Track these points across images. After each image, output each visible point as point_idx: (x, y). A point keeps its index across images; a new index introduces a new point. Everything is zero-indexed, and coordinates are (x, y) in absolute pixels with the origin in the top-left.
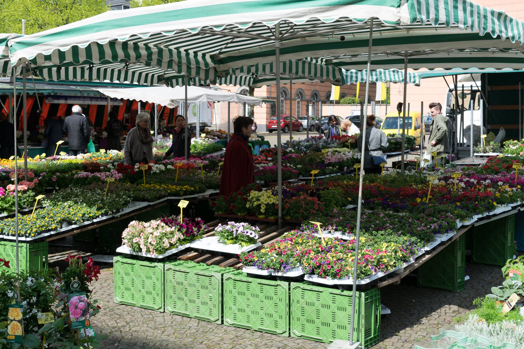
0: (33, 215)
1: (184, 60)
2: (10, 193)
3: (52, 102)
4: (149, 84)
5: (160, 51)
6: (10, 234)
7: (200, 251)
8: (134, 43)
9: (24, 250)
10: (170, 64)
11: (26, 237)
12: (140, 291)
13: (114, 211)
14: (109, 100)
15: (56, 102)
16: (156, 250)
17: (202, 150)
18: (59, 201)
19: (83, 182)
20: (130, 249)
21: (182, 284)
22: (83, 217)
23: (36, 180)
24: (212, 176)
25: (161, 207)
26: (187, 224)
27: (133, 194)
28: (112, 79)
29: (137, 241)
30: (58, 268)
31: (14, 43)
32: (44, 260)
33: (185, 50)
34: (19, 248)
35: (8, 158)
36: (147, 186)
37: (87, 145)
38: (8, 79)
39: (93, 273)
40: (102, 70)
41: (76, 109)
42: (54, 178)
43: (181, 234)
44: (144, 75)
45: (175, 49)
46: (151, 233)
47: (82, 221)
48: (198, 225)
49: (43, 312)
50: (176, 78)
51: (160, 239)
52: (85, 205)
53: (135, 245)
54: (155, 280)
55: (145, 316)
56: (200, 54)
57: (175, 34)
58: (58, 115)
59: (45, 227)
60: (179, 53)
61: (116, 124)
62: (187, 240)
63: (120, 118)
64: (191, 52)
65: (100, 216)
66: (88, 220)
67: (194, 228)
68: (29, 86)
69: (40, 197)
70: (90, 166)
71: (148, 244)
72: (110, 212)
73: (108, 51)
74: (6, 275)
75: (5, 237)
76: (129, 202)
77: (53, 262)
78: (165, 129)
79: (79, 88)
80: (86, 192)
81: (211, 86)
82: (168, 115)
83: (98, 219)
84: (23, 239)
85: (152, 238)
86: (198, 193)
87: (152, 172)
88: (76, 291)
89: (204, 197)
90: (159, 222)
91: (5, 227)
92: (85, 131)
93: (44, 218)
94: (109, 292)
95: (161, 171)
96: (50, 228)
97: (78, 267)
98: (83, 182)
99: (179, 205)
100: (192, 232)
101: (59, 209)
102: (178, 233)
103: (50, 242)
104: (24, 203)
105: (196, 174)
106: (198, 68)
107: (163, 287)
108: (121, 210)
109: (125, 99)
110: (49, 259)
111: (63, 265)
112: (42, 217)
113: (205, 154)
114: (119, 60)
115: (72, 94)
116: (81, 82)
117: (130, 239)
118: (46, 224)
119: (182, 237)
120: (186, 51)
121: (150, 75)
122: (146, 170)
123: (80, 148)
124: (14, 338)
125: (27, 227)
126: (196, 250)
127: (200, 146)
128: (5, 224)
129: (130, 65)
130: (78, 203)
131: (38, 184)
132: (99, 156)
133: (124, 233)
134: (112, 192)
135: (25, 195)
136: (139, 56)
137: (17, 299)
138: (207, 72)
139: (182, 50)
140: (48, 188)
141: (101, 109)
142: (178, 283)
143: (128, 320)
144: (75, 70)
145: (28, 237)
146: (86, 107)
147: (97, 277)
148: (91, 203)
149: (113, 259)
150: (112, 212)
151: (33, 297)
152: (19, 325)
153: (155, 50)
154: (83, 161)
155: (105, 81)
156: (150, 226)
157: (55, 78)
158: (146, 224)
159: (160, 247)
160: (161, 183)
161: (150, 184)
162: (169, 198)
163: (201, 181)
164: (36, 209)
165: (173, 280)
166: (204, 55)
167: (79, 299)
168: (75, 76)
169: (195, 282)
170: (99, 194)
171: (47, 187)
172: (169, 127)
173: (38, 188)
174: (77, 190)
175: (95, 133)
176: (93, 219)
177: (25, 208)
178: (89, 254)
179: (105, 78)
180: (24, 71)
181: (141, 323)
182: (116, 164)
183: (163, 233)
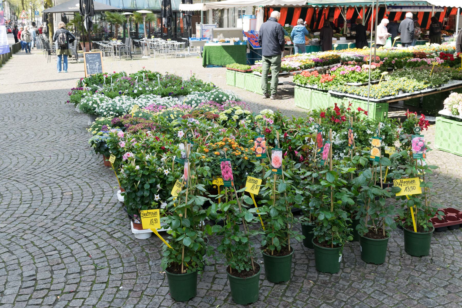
13: (437, 85)
14: (434, 8)
15: (394, 10)
18: (397, 77)
19: (414, 65)
23: (381, 62)
35: (361, 48)
39: (424, 125)
41: (409, 15)
42: (393, 62)
49: (388, 146)
53: (454, 110)
55: (458, 161)
58: (395, 20)
63: (440, 21)
66: (417, 90)
70: (418, 55)
72: (434, 86)
74: (366, 119)
84: (373, 100)
91: (361, 91)
96: (391, 94)
98: (414, 65)
103: (390, 103)
109: (447, 6)
111: (403, 119)
115: (407, 5)
117: (450, 105)
124: (374, 158)
133: (445, 100)
134: (435, 72)
135: (374, 72)
141: (427, 15)
143: (445, 161)
146: (415, 13)
152: (378, 150)
170: (426, 73)
174: (409, 70)
175: (421, 32)
176: (421, 90)
181: (454, 165)
182: (439, 53)
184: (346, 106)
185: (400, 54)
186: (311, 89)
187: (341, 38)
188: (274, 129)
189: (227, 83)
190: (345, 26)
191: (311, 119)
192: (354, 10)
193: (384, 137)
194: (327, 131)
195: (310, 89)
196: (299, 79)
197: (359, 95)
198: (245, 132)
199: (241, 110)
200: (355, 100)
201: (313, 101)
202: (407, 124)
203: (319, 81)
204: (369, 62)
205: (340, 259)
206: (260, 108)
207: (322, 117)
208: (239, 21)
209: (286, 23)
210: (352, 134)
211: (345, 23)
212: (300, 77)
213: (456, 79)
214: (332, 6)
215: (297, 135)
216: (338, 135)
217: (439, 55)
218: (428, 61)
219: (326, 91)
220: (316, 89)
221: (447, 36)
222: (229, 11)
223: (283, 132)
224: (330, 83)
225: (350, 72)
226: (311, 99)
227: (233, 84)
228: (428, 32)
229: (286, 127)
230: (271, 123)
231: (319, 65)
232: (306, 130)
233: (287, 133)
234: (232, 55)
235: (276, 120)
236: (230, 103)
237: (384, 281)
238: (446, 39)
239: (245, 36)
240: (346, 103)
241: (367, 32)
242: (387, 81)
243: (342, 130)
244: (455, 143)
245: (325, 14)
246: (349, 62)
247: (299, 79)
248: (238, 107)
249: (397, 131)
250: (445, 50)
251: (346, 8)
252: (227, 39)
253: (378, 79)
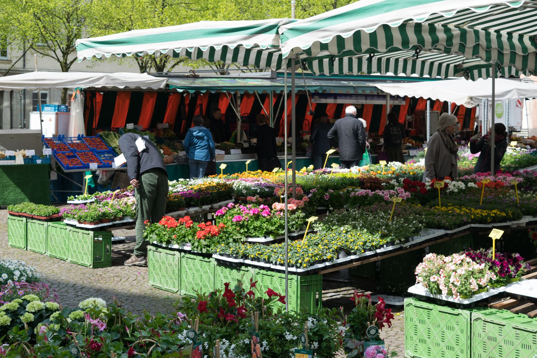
0: (304, 241)
1: (494, 44)
2: (276, 213)
3: (318, 102)
4: (444, 77)
5: (463, 34)
6: (278, 263)
7: (519, 298)
8: (429, 24)
9: (294, 283)
10: (476, 51)
11: (297, 267)
12: (438, 345)
13: (403, 240)
14: (389, 98)
15: (323, 101)
16: (461, 293)
17: (512, 163)
18: (334, 225)
19: (361, 202)
20: (426, 289)
21: (495, 339)
22: (363, 245)
23: (306, 198)
24: (529, 198)
25: (462, 237)
26: (501, 261)
27: (426, 219)
28: (396, 72)
29: (436, 279)
30: (342, 309)
31: (286, 30)
32: (317, 296)
33: (496, 31)
34: (289, 281)
35: (270, 170)
36: (444, 209)
37: (362, 155)
38: (268, 74)
40: (384, 60)
41: (351, 110)
43: (493, 273)
44: (436, 64)
45: (482, 29)
46: (453, 271)
47: (363, 251)
48: (516, 262)
50: (479, 67)
51: (466, 278)
52: (365, 230)
53: (432, 285)
54: (459, 332)
56: (516, 36)
57: (491, 8)
59: (318, 257)
60: (488, 34)
61: (395, 129)
62: (501, 282)
63: (401, 121)
64: (504, 33)
65: (385, 246)
67: (510, 266)
68: (300, 82)
69: (312, 219)
70: (368, 182)
71: (450, 285)
72: (397, 241)
73: (397, 37)
74: (283, 312)
75: (273, 267)
76: (421, 229)
77: (327, 300)
78: (459, 136)
79: (351, 84)
80: (366, 214)
81: (522, 76)
82: (463, 117)
83: (382, 249)
84: (293, 269)
85: (455, 276)
86: (510, 220)
87: (448, 191)
88: (373, 339)
89: (519, 226)
90: (463, 256)
91: (273, 255)
92: (360, 137)
93: (317, 245)
94: (397, 343)
95: (460, 190)
97: (367, 309)
98: (361, 202)
99: (490, 236)
100: (508, 271)
101: (334, 235)
102: (489, 272)
103: (324, 275)
104: (293, 225)
105: (508, 194)
106: (513, 54)
107: (469, 342)
108: (410, 239)
109: (410, 96)
110: (323, 296)
111: (348, 304)
112: (315, 244)
113: (516, 168)
114: (411, 46)
115: (344, 91)
116: (358, 76)
117: (426, 277)
118: (320, 252)
119: (495, 278)
120: (497, 31)
121: (444, 65)
122: (441, 189)
123: (354, 158)
125: (298, 255)
126: (513, 296)
127: (509, 158)
128: (272, 251)
129: (422, 52)
130: (357, 228)
131: (308, 202)
132: (378, 170)
133: (417, 268)
134: (398, 215)
135: (293, 216)
136: (435, 41)
137: (304, 343)
138: (525, 59)
139: (492, 30)
140: (319, 208)
141: (378, 109)
142: (490, 338)
144: (350, 60)
145: (299, 268)
147: (390, 322)
148: (373, 229)
149: (403, 301)
150: (400, 240)
151: (314, 343)
153: (456, 32)
154: (359, 175)
155: (388, 74)
156: (452, 261)
157: (326, 72)
158: (447, 259)
159: (466, 289)
160: (460, 206)
161: (447, 206)
162: (473, 225)
163: (514, 205)
164: (307, 234)
165: (483, 334)
166: (521, 37)
167: (377, 350)
168: (350, 69)
169: (513, 339)
170: (382, 218)
171: (318, 207)
172: (463, 132)
173: (308, 208)
174: (355, 212)
176: (376, 248)
177: (294, 232)
178: (370, 293)
179: (387, 70)
180: (293, 63)
182: (402, 179)
183: (469, 271)
184: (246, 286)
185: (338, 180)
186: (180, 251)
187: (232, 151)
188: (108, 341)
189: (10, 243)
190: (239, 127)
191: (181, 315)
192: (253, 99)
193: (316, 344)
194: (210, 339)
195: (176, 253)
196: (157, 232)
197: (268, 262)
198: (48, 351)
199: (39, 302)
200: (262, 271)
201: (184, 276)
202: (355, 317)
203: (193, 236)
204: (283, 199)
206: (79, 293)
207: (201, 311)
208: (34, 118)
209: (128, 122)
210: (258, 345)
211: (239, 123)
212: (157, 228)
213: (432, 228)
214: (213, 92)
215: (154, 352)
216: (233, 346)
217: (402, 183)
218: (384, 194)
219: (209, 256)
220: (189, 252)
221: (413, 148)
222: (14, 95)
223: (125, 346)
224: (216, 239)
225: (251, 217)
226: (180, 270)
227: (22, 245)
228: (382, 140)
229: (132, 335)
230: (102, 329)
231: (192, 203)
232: (171, 339)
233: (135, 348)
234: (21, 184)
235: (111, 321)
236: (14, 288)
238: (412, 152)
239: (47, 147)
240: (246, 277)
241: (278, 140)
242: (318, 233)
243: (240, 335)
244: (438, 345)
245: (201, 105)
246: (249, 198)
247: (157, 232)
248: (33, 296)
249: (339, 332)
250: (411, 173)
251: (239, 95)
252: (8, 153)
253: (301, 230)
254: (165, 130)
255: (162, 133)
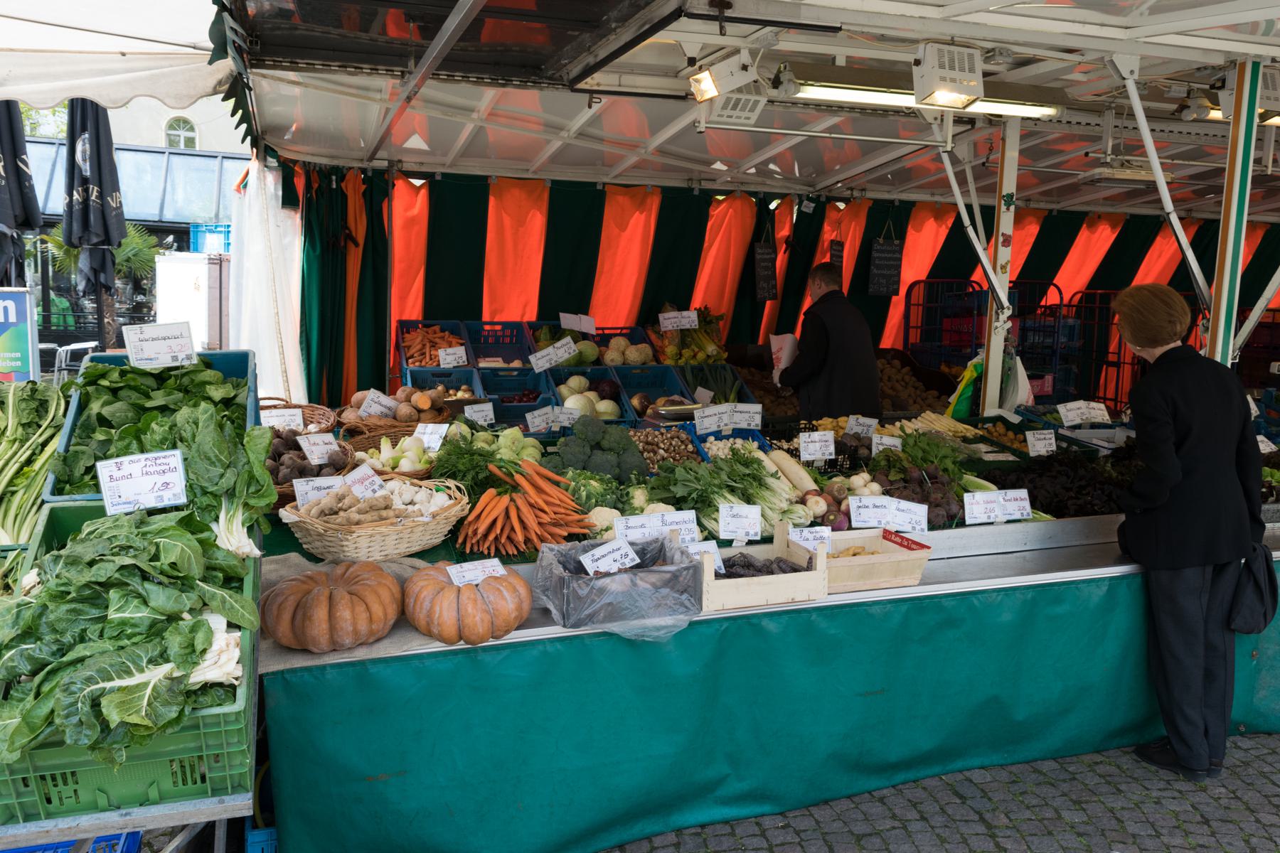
205: (1254, 410)
237: (67, 791)
245: (837, 245)
254: (685, 336)
255: (671, 350)
